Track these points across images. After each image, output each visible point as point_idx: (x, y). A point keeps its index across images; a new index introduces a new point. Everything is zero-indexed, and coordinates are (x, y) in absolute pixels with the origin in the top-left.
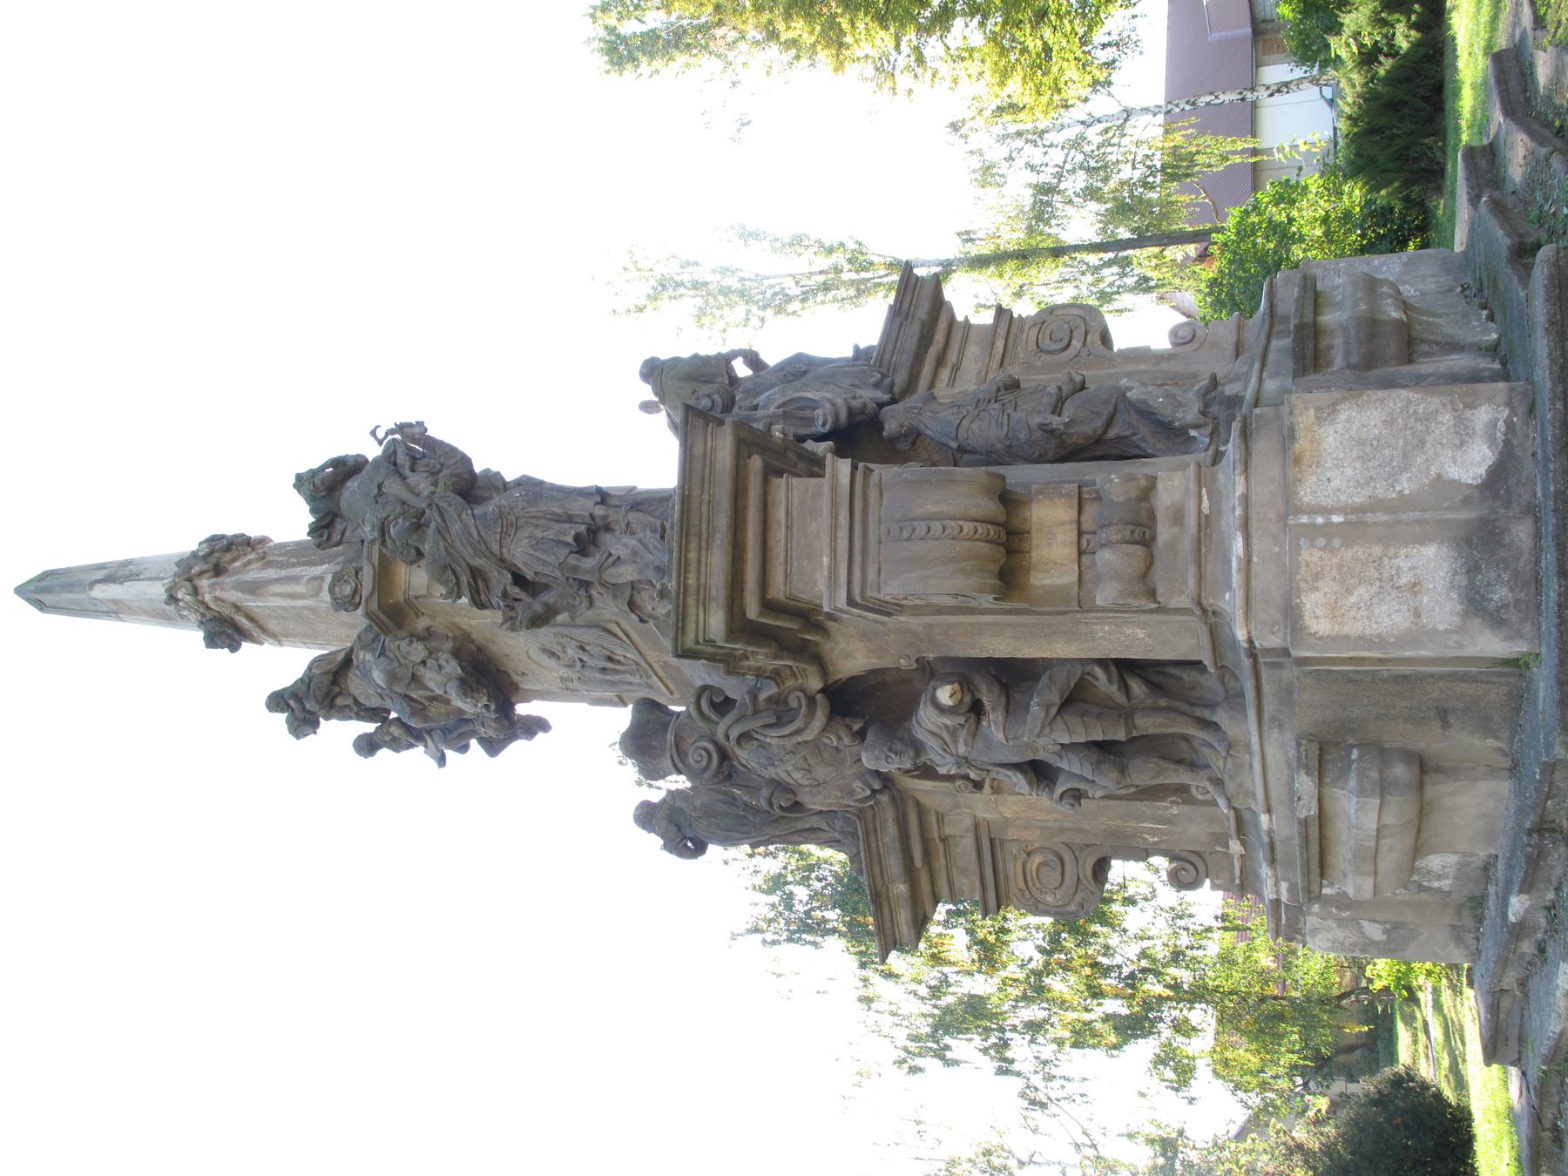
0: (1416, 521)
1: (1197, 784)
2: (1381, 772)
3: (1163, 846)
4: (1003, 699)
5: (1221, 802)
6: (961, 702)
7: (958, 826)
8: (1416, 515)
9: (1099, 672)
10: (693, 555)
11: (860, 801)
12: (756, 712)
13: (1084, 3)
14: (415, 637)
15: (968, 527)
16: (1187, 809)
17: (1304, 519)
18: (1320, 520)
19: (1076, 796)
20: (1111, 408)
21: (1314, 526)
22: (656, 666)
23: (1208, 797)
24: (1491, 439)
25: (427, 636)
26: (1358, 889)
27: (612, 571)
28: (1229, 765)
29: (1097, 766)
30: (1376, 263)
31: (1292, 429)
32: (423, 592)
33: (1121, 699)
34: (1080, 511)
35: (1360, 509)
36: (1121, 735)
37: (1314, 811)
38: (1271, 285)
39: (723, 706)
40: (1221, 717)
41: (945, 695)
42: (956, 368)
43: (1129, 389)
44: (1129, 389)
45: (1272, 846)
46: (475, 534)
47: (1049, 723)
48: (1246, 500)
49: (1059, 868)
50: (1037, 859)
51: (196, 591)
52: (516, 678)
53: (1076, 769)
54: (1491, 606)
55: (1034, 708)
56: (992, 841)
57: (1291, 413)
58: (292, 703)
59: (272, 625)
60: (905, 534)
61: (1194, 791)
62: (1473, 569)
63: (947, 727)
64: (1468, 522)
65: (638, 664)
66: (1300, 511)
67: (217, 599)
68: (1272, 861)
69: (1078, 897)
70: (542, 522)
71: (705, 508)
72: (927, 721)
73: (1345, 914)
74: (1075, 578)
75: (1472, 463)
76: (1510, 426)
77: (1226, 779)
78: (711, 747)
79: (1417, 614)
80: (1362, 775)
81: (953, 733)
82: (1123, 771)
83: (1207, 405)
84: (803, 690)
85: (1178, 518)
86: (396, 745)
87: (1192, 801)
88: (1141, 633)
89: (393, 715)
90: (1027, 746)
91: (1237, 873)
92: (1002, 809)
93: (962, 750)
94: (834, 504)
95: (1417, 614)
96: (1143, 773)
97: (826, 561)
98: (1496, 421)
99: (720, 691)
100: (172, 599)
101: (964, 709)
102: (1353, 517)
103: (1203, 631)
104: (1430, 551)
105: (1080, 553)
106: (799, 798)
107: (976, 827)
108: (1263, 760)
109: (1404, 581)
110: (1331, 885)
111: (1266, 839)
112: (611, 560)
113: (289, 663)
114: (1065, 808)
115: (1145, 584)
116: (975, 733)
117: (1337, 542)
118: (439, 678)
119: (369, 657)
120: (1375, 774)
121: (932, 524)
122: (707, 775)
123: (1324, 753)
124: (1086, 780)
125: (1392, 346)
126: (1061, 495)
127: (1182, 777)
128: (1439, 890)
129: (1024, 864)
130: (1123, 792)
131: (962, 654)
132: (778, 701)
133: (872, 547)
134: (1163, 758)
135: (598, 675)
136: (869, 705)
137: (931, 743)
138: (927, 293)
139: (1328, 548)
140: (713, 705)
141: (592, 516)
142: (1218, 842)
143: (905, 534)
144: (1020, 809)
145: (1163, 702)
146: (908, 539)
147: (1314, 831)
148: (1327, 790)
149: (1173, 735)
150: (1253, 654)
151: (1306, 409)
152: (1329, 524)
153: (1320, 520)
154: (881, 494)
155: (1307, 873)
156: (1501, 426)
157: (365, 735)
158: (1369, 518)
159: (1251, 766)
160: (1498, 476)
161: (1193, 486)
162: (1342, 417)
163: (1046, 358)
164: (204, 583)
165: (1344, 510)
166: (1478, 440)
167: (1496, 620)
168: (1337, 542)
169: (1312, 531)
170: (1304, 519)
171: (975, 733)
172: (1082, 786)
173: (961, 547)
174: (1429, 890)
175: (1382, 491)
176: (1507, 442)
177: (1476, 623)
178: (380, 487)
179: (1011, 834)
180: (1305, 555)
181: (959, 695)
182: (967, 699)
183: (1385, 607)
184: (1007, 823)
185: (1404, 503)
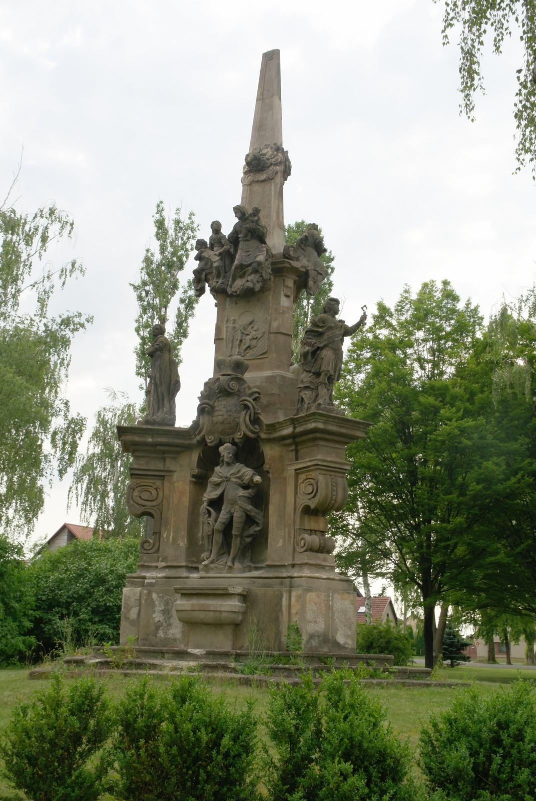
10: (336, 421)
13: (2, 593)
24: (345, 643)
33: (246, 533)
35: (332, 610)
37: (231, 592)
50: (154, 492)
56: (164, 476)
75: (341, 640)
79: (310, 622)
85: (325, 560)
91: (150, 564)
94: (338, 463)
95: (310, 622)
104: (323, 626)
105: (311, 530)
107: (170, 471)
118: (255, 280)
122: (227, 387)
133: (323, 472)
139: (325, 600)
159: (257, 569)
160: (338, 644)
165: (332, 605)
167: (308, 642)
173: (330, 495)
175: (336, 615)
178: (321, 274)
180: (323, 594)
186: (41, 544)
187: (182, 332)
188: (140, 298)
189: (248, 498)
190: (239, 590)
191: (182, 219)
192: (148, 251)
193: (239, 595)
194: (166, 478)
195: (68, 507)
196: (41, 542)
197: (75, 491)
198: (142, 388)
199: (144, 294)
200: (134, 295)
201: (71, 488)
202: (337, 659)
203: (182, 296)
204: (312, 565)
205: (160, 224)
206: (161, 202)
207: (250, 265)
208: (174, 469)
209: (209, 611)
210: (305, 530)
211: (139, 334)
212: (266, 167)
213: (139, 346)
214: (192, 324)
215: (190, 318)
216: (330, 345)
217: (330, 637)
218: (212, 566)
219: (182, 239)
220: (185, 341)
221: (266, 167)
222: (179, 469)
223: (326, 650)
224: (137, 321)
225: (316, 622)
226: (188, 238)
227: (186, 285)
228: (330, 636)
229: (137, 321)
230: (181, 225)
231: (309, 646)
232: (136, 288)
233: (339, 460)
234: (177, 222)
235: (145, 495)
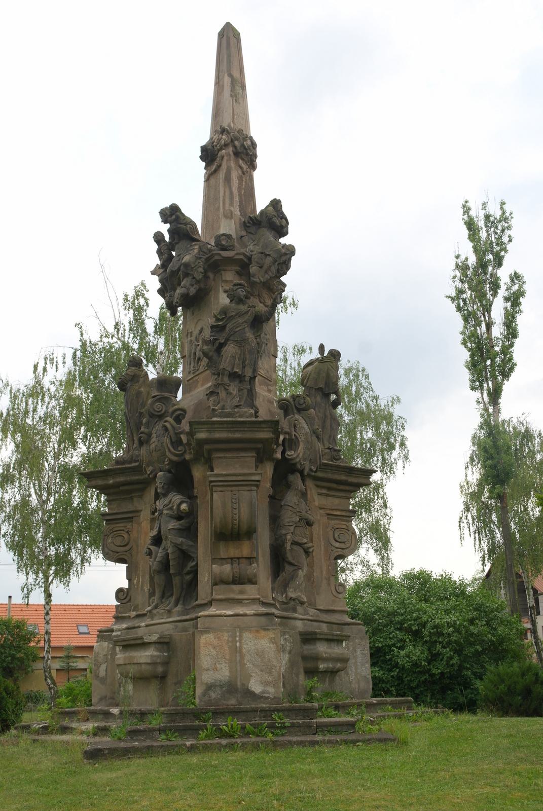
0: (237, 669)
1: (156, 599)
2: (159, 663)
3: (132, 586)
4: (183, 528)
5: (149, 608)
6: (182, 512)
7: (137, 504)
8: (239, 668)
9: (194, 563)
11: (145, 469)
12: (176, 434)
14: (206, 272)
15: (236, 522)
16: (147, 595)
17: (238, 634)
18: (237, 639)
19: (150, 553)
20: (296, 564)
21: (236, 637)
22: (197, 377)
23: (151, 603)
24: (263, 692)
25: (206, 277)
26: (119, 658)
27: (223, 389)
28: (162, 611)
29: (160, 562)
30: (367, 665)
31: (268, 630)
32: (224, 278)
33: (185, 571)
34: (246, 558)
36: (172, 571)
38: (359, 624)
39: (178, 420)
40: (179, 608)
41: (184, 506)
42: (327, 495)
43: (303, 571)
44: (303, 571)
45: (134, 628)
46: (237, 330)
47: (175, 545)
48: (245, 615)
49: (122, 544)
50: (126, 536)
51: (226, 145)
52: (192, 309)
53: (159, 555)
54: (210, 692)
55: (181, 539)
56: (132, 518)
57: (273, 629)
58: (174, 217)
59: (212, 180)
60: (234, 501)
61: (153, 598)
62: (221, 686)
63: (173, 506)
64: (237, 685)
65: (198, 370)
66: (241, 632)
67: (223, 157)
68: (128, 628)
69: (110, 552)
70: (242, 356)
71: (242, 429)
72: (176, 498)
73: (109, 657)
74: (223, 557)
75: (256, 687)
76: (268, 698)
77: (157, 610)
78: (163, 412)
79: (207, 670)
80: (158, 657)
81: (171, 509)
82: (159, 572)
83: (294, 600)
84: (185, 452)
85: (241, 592)
86: (159, 252)
87: (150, 598)
88: (206, 579)
89: (174, 253)
90: (167, 537)
91: (124, 615)
92: (145, 522)
93: (165, 512)
94: (244, 475)
95: (207, 670)
96: (159, 579)
97: (225, 472)
98: (269, 693)
99: (184, 418)
100: (223, 131)
101: (180, 513)
102: (238, 649)
103: (205, 601)
104: (227, 673)
105: (232, 559)
106: (145, 445)
108: (162, 623)
109: (218, 665)
110: (120, 651)
111: (136, 625)
112: (227, 387)
113: (194, 211)
114: (145, 550)
115: (218, 581)
116: (171, 517)
117: (230, 644)
118: (188, 285)
119: (196, 251)
120: (158, 661)
121: (237, 510)
123: (165, 643)
124: (155, 558)
125: (310, 665)
126: (252, 551)
127: (157, 595)
128: (120, 691)
129: (123, 530)
130: (152, 572)
131: (199, 513)
132: (180, 442)
133: (230, 488)
134: (165, 587)
135: (193, 351)
136: (180, 479)
137: (167, 501)
138: (362, 480)
139: (228, 642)
140: (179, 415)
141: (245, 376)
142: (134, 608)
143: (234, 501)
144: (144, 532)
145: (185, 586)
146: (232, 502)
147: (139, 642)
148: (153, 645)
149: (173, 590)
150: (197, 618)
151: (275, 634)
152: (236, 642)
153: (237, 639)
154: (248, 491)
155: (124, 640)
156: (267, 695)
157: (164, 237)
158: (238, 655)
160: (252, 694)
161: (252, 597)
162: (272, 646)
163: (331, 533)
164: (230, 150)
166: (263, 688)
167: (205, 693)
168: (230, 644)
169: (234, 636)
170: (238, 634)
171: (171, 517)
172: (153, 556)
174: (120, 686)
175: (247, 658)
176: (262, 697)
177: (204, 687)
178: (269, 255)
179: (135, 525)
180: (226, 634)
181: (184, 512)
182: (183, 515)
183: (209, 660)
184: (139, 524)
185: (243, 665)
186: (480, 578)
187: (511, 332)
188: (459, 309)
189: (179, 530)
190: (154, 638)
191: (492, 212)
192: (457, 257)
193: (155, 643)
194: (134, 519)
195: (462, 538)
196: (479, 576)
197: (465, 521)
198: (479, 402)
199: (462, 304)
200: (452, 307)
201: (461, 518)
202: (213, 713)
203: (506, 294)
204: (221, 600)
205: (471, 225)
206: (466, 202)
207: (179, 269)
208: (140, 509)
209: (134, 664)
210: (222, 559)
211: (466, 347)
212: (229, 152)
213: (469, 359)
214: (521, 321)
215: (518, 315)
216: (232, 338)
217: (239, 687)
218: (155, 611)
219: (496, 233)
220: (517, 342)
221: (229, 152)
222: (144, 507)
223: (233, 702)
224: (462, 333)
225: (215, 669)
226: (503, 231)
227: (508, 280)
228: (239, 684)
229: (462, 333)
230: (492, 219)
231: (206, 698)
232: (453, 299)
233: (246, 471)
234: (487, 217)
235: (118, 541)
